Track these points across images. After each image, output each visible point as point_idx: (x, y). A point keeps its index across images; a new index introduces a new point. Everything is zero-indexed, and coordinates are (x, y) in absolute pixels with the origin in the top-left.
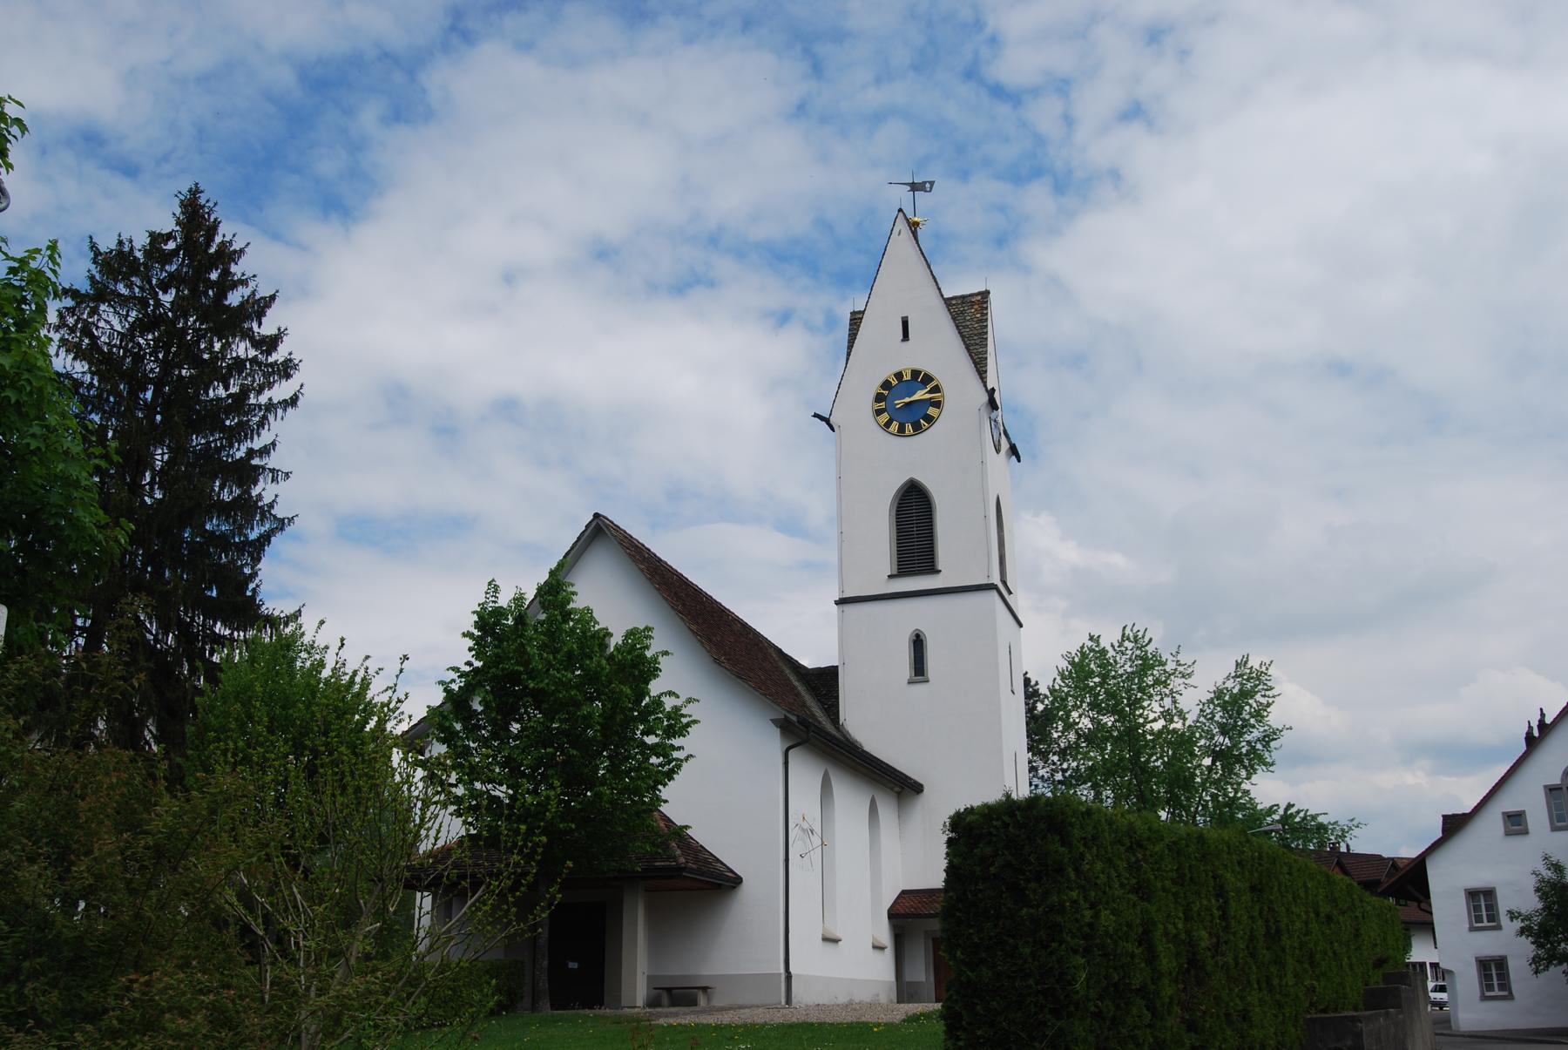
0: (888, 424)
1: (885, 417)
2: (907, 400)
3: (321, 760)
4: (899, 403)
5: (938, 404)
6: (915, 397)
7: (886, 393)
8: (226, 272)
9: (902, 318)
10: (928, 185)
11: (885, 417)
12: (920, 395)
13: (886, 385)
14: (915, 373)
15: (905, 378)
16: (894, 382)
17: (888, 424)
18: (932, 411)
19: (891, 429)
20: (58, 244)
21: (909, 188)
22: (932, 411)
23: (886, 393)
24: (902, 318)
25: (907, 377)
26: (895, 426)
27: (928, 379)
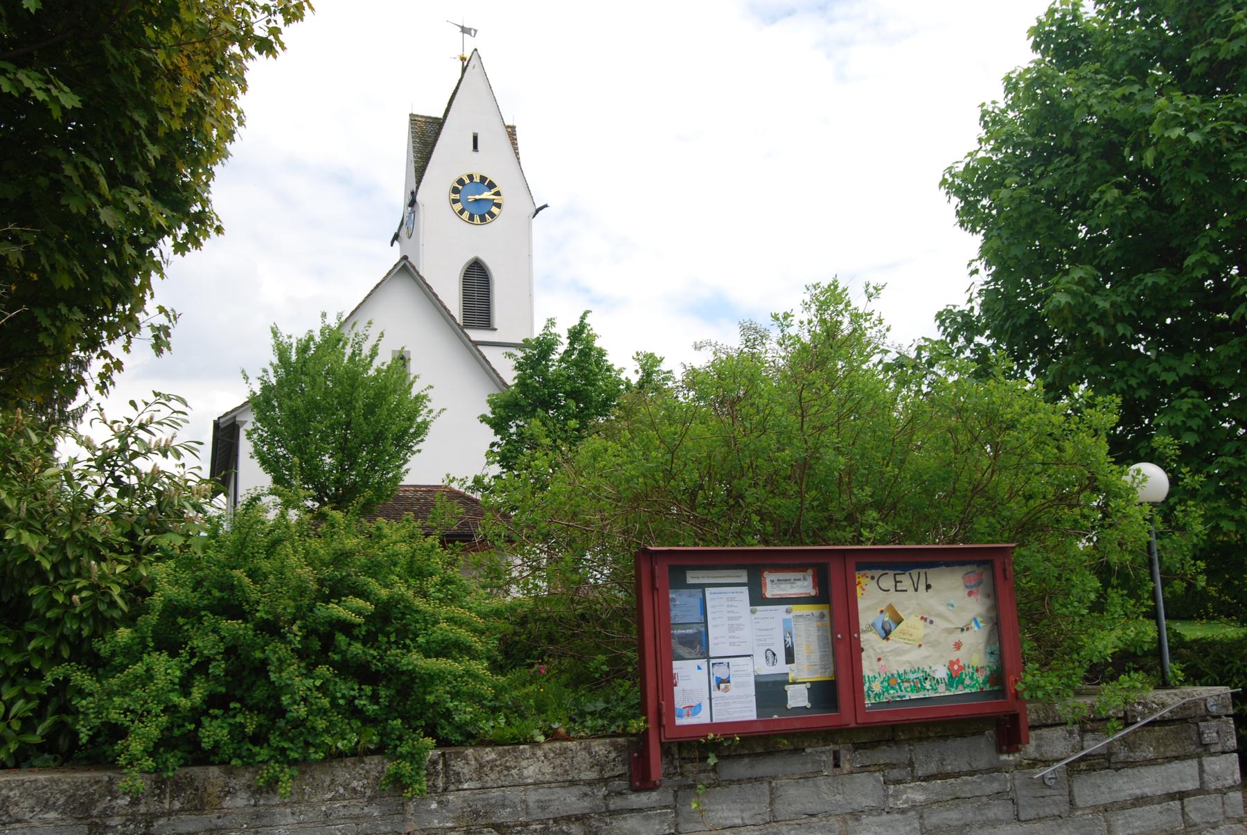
0: (461, 212)
1: (458, 206)
2: (477, 197)
3: (282, 771)
4: (471, 198)
5: (499, 206)
6: (482, 196)
7: (460, 187)
8: (1013, 356)
9: (793, 662)
10: (473, 32)
11: (458, 206)
12: (487, 195)
13: (461, 182)
14: (483, 179)
15: (475, 180)
16: (467, 181)
17: (461, 212)
18: (494, 210)
19: (463, 217)
20: (414, 368)
21: (460, 29)
22: (494, 210)
23: (460, 187)
24: (793, 662)
25: (477, 180)
26: (466, 215)
27: (491, 185)
